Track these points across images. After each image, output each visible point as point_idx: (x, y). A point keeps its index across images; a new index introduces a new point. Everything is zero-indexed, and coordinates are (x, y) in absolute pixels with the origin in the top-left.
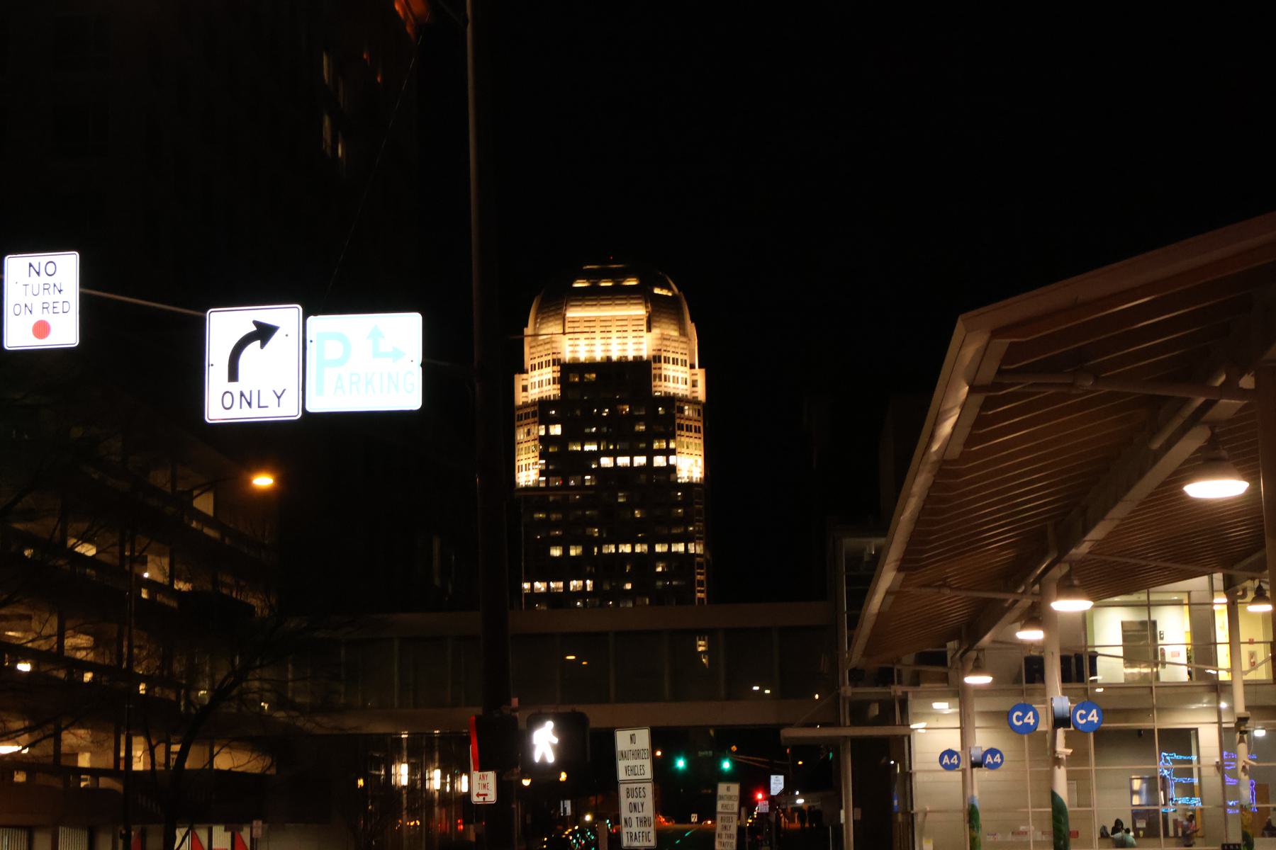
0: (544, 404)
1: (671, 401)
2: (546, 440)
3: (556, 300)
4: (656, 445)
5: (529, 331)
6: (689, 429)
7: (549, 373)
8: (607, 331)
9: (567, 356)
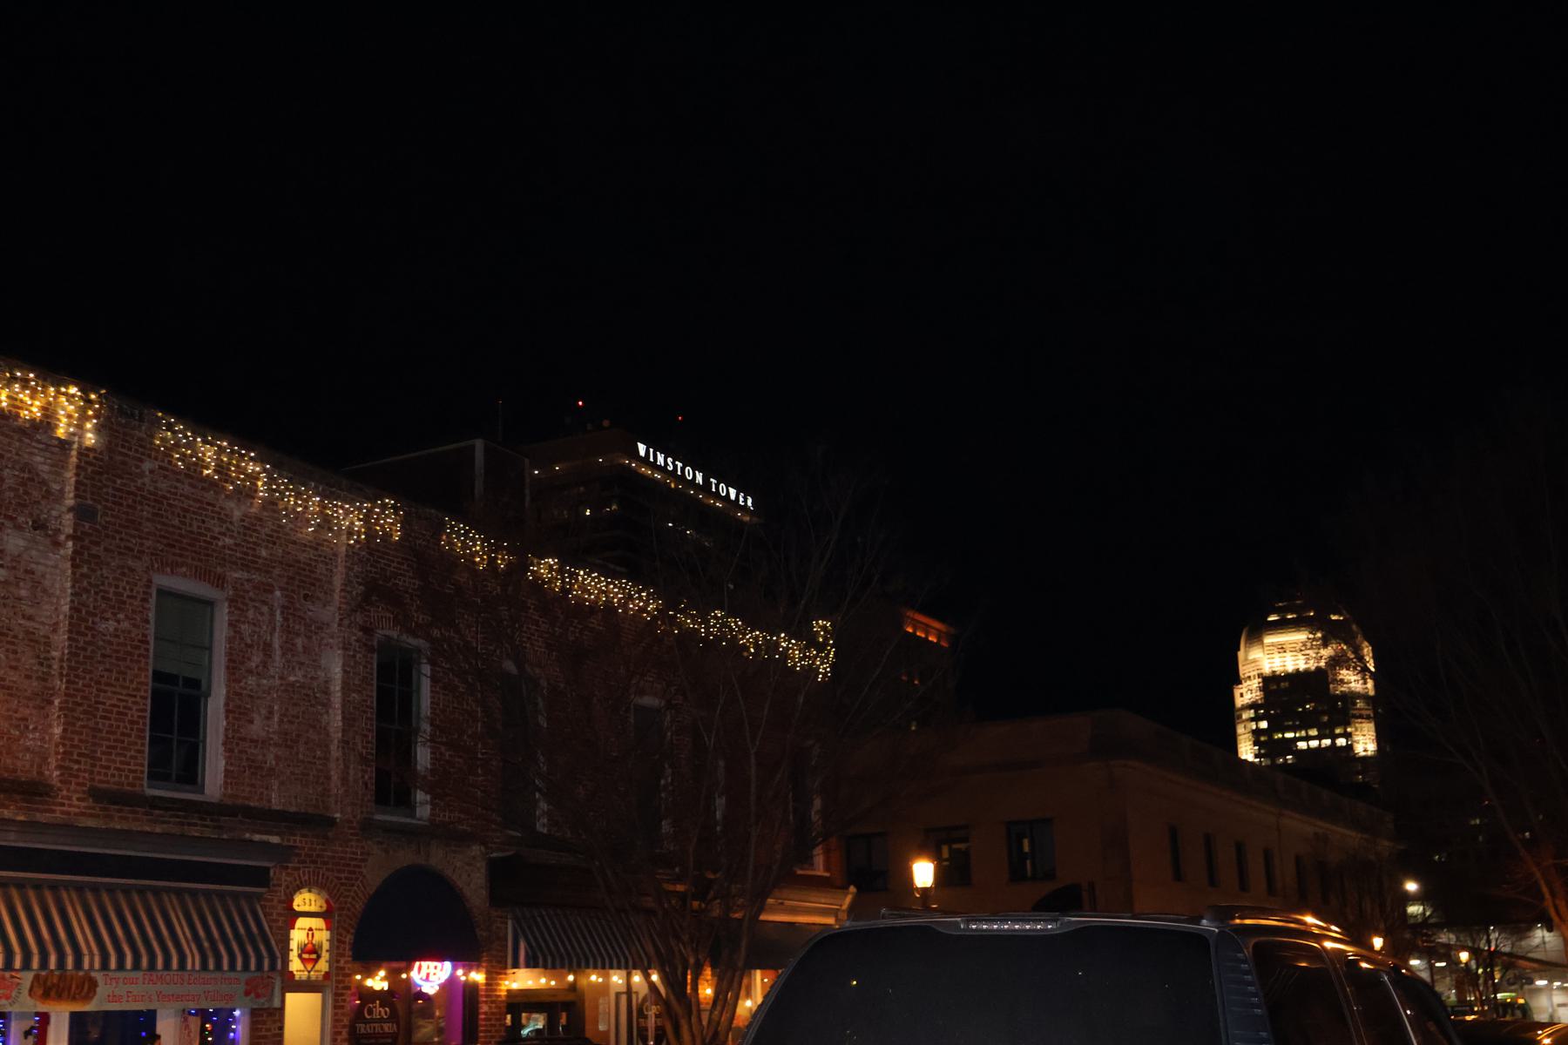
0: (1253, 706)
1: (1350, 697)
2: (1257, 733)
3: (1258, 630)
4: (1338, 731)
5: (1241, 654)
6: (1361, 717)
7: (1255, 683)
8: (1280, 653)
9: (1267, 670)
